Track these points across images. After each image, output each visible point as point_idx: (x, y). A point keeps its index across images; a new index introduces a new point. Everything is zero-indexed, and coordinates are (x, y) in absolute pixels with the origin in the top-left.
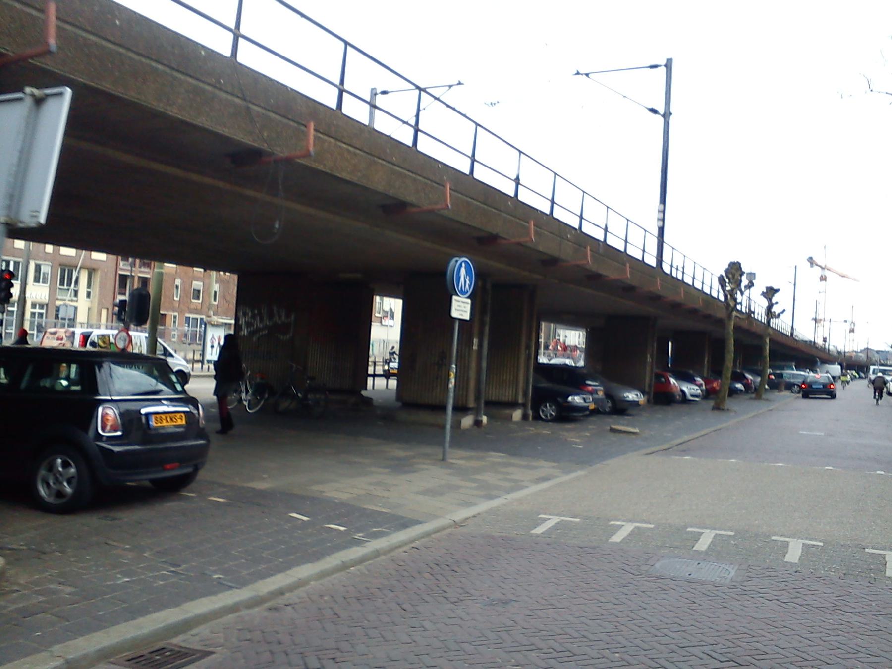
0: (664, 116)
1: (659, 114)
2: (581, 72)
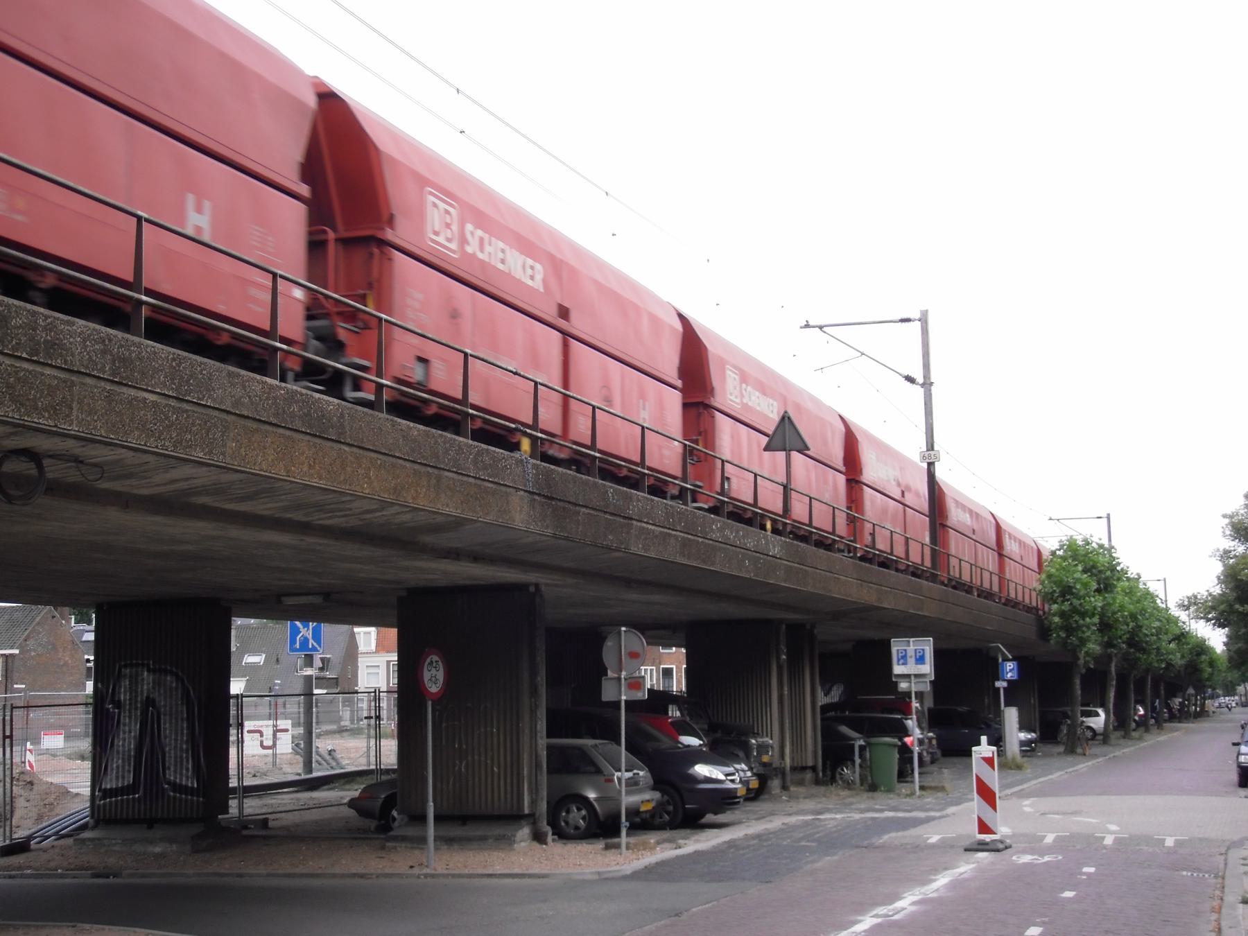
0: (923, 385)
1: (918, 384)
2: (811, 323)
